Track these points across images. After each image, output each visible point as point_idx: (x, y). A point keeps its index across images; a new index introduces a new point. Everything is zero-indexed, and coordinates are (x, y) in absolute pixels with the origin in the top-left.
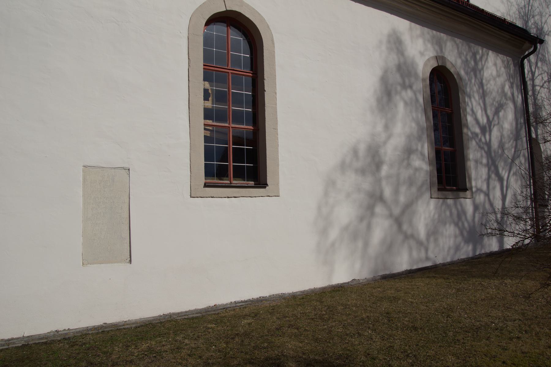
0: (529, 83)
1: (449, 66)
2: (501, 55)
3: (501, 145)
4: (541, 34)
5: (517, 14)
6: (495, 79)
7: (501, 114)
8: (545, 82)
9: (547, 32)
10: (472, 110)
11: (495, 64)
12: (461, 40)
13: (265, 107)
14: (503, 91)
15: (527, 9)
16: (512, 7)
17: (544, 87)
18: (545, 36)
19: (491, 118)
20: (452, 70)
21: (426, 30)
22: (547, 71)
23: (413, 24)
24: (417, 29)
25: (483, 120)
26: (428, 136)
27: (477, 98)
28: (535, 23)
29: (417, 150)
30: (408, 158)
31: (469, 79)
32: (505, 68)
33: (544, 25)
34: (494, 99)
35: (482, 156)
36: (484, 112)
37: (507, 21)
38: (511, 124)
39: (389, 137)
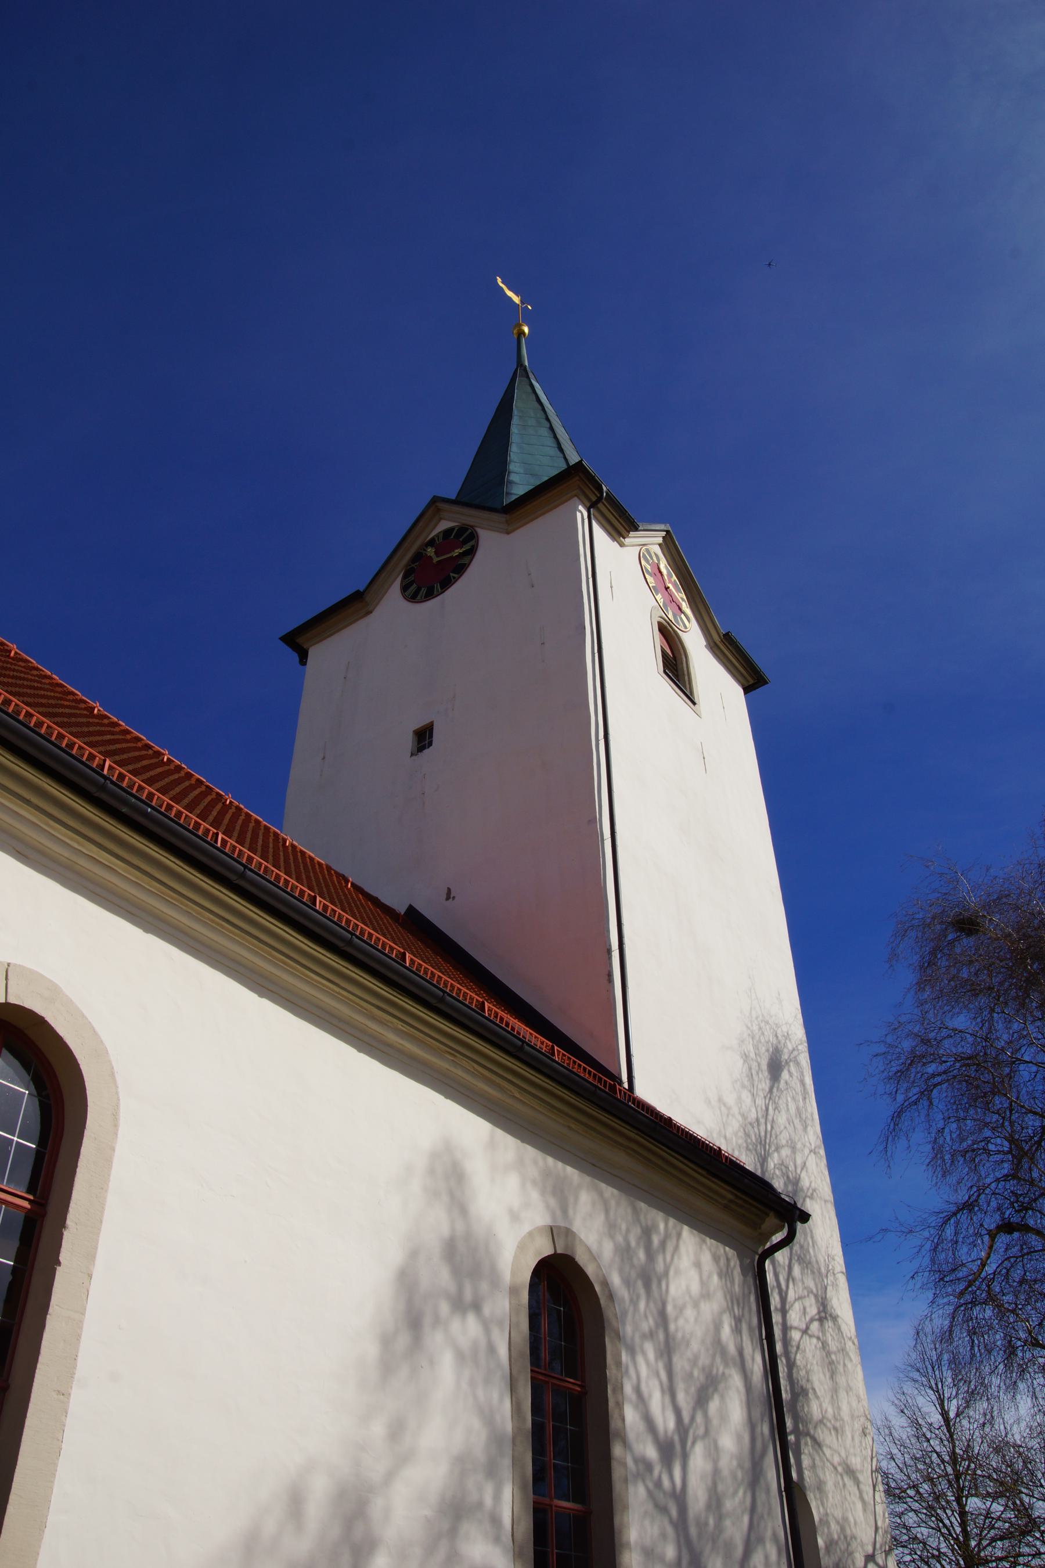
0: (776, 1318)
1: (581, 1258)
2: (712, 1240)
3: (715, 1501)
4: (795, 1192)
5: (741, 1137)
6: (696, 1305)
7: (713, 1406)
8: (812, 1320)
9: (808, 1189)
10: (638, 1390)
11: (698, 1265)
12: (615, 1191)
13: (48, 1316)
14: (717, 1342)
15: (762, 1128)
16: (730, 1117)
17: (810, 1332)
18: (804, 1200)
19: (686, 1417)
20: (590, 1270)
21: (530, 1152)
22: (814, 1290)
23: (499, 1133)
24: (509, 1145)
25: (665, 1422)
26: (516, 1461)
27: (651, 1355)
28: (782, 1164)
29: (480, 1504)
30: (453, 1532)
31: (631, 1300)
32: (720, 1276)
33: (801, 1172)
34: (694, 1361)
35: (663, 1535)
36: (667, 1399)
37: (724, 1155)
38: (739, 1437)
39: (403, 1460)
